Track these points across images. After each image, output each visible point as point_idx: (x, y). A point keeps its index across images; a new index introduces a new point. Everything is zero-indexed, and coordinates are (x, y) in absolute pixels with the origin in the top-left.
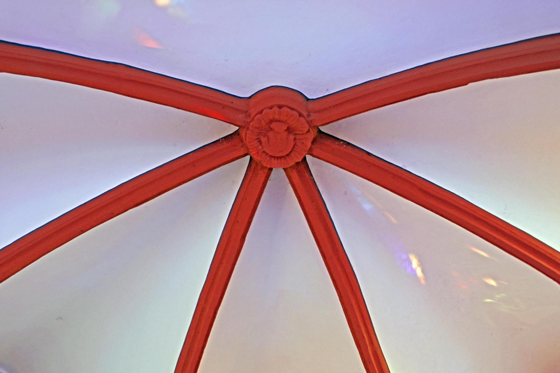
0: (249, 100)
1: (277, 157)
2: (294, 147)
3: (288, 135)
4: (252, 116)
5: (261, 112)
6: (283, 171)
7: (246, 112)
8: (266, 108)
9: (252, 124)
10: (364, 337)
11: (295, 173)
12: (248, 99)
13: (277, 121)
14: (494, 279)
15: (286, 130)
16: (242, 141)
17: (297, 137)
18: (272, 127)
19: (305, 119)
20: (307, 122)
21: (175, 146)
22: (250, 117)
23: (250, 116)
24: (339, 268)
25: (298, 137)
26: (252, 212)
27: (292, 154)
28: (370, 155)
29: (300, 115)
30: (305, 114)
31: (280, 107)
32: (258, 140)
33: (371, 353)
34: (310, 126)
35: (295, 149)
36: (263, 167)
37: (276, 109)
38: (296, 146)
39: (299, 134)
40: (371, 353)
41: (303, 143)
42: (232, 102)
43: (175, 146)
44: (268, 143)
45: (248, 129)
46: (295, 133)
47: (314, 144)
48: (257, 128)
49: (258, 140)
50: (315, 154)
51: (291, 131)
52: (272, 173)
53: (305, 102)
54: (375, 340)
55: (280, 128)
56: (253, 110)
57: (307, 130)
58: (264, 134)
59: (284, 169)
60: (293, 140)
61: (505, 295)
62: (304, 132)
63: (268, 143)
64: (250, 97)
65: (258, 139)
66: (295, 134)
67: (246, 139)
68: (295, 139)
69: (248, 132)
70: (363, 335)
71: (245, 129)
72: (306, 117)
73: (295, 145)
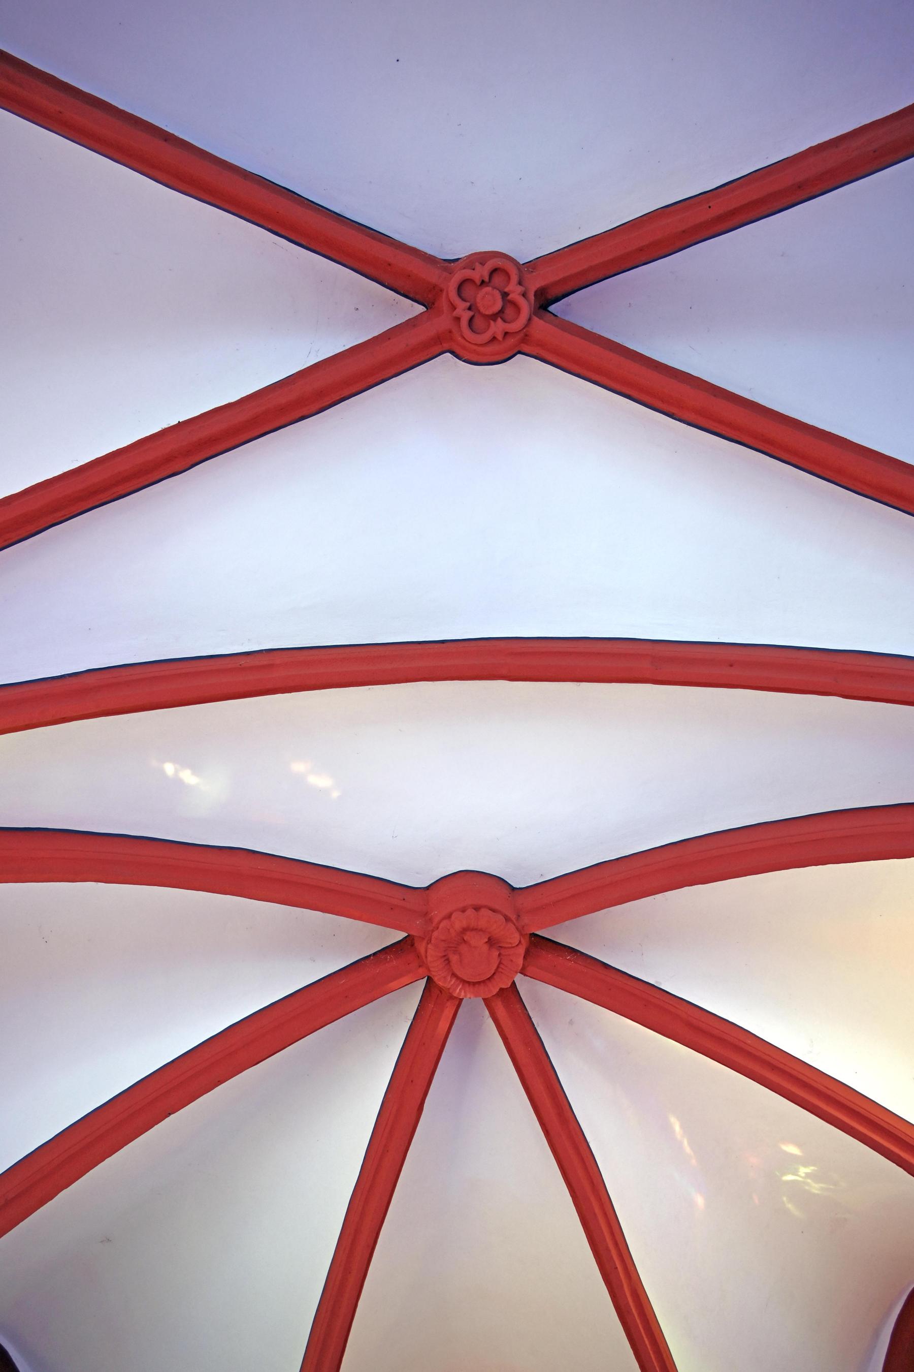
0: (427, 892)
1: (473, 982)
2: (498, 967)
3: (489, 949)
4: (436, 920)
5: (449, 917)
6: (482, 1002)
7: (426, 914)
8: (455, 911)
9: (435, 934)
10: (617, 1268)
11: (500, 1003)
12: (425, 891)
13: (473, 929)
14: (799, 1145)
15: (486, 942)
16: (419, 956)
17: (503, 951)
18: (465, 939)
19: (515, 925)
20: (517, 929)
21: (314, 961)
22: (432, 923)
23: (431, 920)
24: (581, 1173)
25: (503, 951)
26: (437, 1059)
27: (495, 977)
28: (606, 968)
29: (507, 919)
30: (513, 917)
31: (477, 908)
32: (444, 959)
33: (628, 1294)
34: (521, 935)
35: (500, 970)
36: (451, 997)
37: (470, 912)
38: (501, 966)
39: (505, 948)
40: (628, 1294)
41: (512, 961)
42: (404, 899)
43: (314, 961)
44: (461, 962)
45: (429, 941)
46: (500, 945)
47: (526, 959)
48: (444, 941)
49: (444, 959)
50: (528, 975)
51: (493, 942)
52: (230, 161)
53: (510, 898)
54: (632, 1268)
55: (479, 941)
56: (436, 912)
57: (518, 941)
58: (453, 949)
59: (484, 1000)
60: (497, 956)
61: (816, 1169)
62: (513, 945)
63: (461, 962)
64: (428, 888)
65: (445, 956)
66: (499, 947)
67: (426, 957)
68: (500, 955)
69: (429, 946)
70: (615, 1265)
71: (425, 941)
72: (515, 921)
73: (500, 963)
